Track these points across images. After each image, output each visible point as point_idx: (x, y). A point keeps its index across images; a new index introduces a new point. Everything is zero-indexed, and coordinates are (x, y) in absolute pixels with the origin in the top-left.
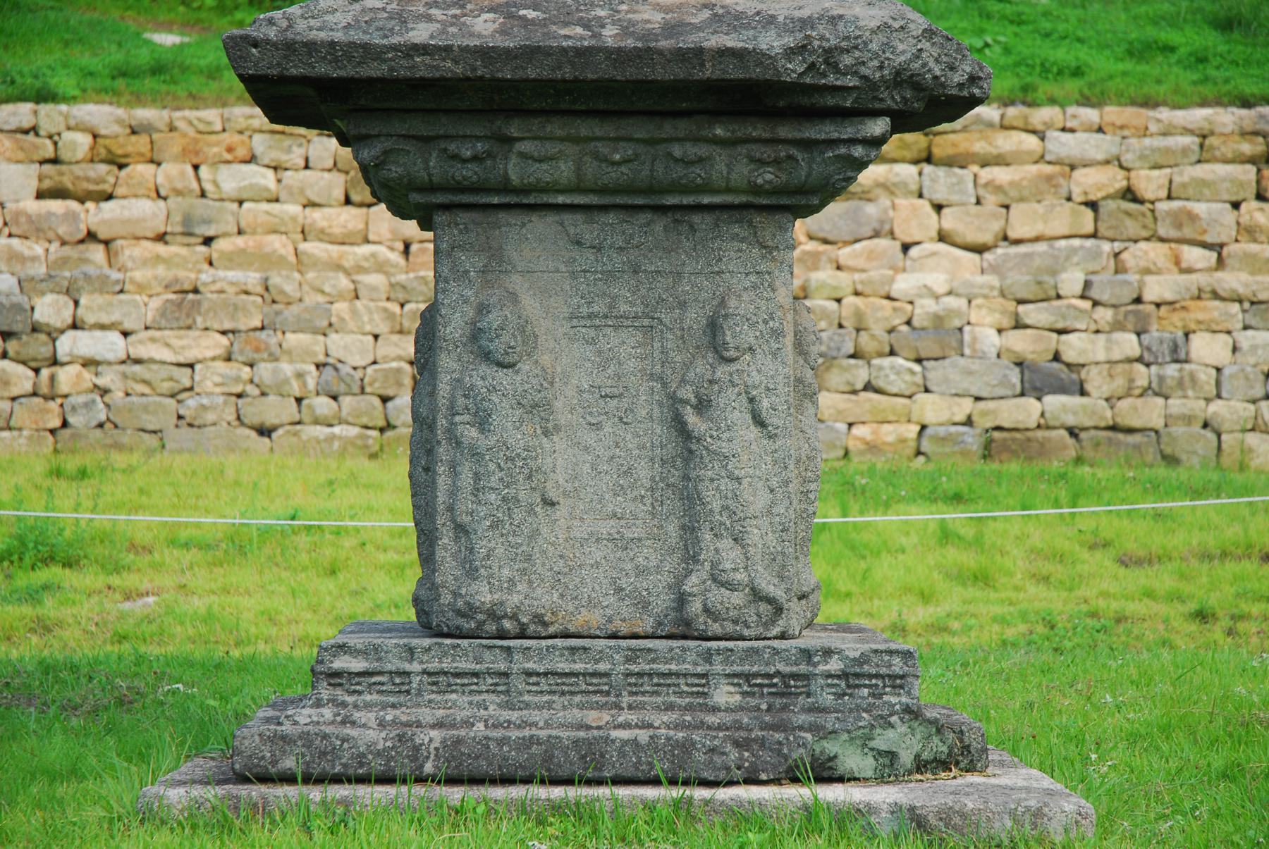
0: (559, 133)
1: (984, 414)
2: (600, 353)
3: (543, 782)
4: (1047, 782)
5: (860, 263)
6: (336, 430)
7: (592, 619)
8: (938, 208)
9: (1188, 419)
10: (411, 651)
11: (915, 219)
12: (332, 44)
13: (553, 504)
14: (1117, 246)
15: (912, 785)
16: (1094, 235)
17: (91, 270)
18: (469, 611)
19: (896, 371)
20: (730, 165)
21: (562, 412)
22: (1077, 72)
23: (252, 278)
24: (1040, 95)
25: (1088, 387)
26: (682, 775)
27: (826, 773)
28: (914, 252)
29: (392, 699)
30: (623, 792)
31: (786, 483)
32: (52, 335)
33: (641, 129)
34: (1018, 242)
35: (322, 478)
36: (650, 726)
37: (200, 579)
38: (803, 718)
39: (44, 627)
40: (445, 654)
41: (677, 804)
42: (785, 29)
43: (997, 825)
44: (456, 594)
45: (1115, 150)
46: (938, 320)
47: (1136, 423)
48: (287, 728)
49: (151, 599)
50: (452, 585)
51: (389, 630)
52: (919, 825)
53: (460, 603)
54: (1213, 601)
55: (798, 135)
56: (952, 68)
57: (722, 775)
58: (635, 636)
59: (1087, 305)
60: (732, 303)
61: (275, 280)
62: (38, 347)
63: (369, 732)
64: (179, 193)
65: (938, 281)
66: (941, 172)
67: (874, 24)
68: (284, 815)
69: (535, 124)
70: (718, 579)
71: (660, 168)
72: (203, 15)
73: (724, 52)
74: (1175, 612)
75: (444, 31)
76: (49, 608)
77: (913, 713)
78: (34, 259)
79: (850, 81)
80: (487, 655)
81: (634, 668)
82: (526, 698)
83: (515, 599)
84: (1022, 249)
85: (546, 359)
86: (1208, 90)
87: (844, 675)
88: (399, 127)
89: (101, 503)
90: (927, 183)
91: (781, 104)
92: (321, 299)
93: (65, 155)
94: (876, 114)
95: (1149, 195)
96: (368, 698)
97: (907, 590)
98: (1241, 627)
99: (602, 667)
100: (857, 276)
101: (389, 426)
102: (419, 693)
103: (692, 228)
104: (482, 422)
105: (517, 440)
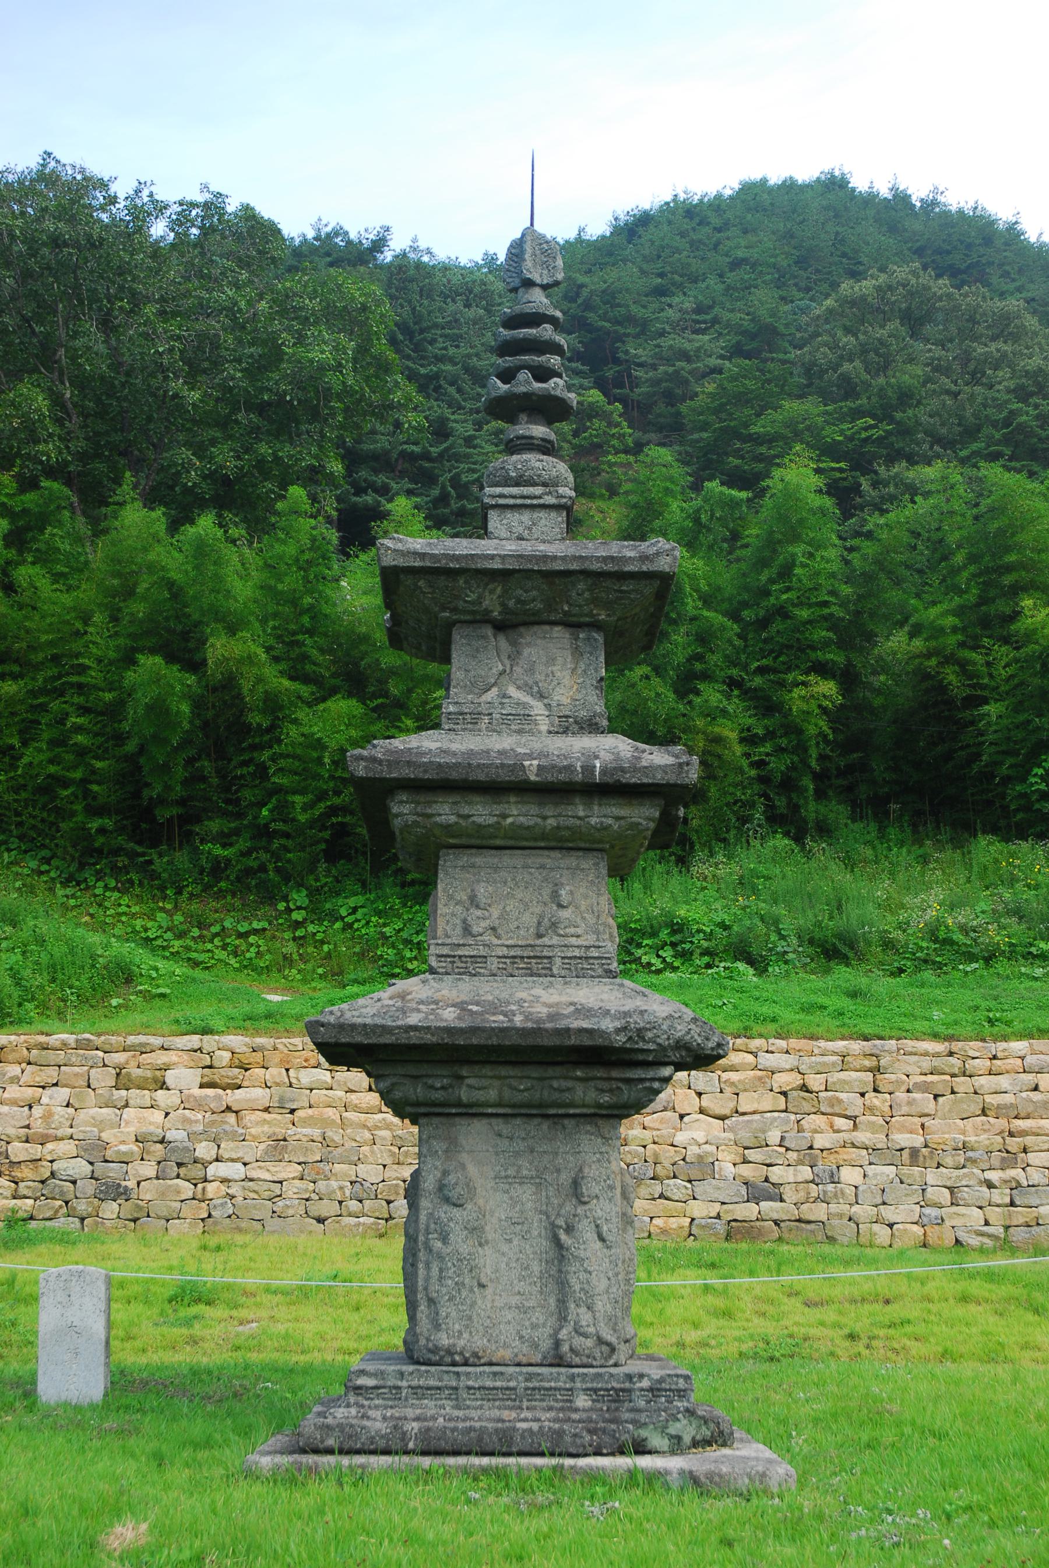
0: (490, 1074)
2: (511, 1198)
3: (477, 1454)
4: (768, 1454)
5: (656, 1125)
6: (361, 1220)
7: (506, 1354)
8: (699, 1094)
9: (840, 1216)
10: (402, 1374)
12: (365, 1025)
13: (484, 1286)
14: (799, 1117)
16: (786, 1111)
17: (227, 1128)
18: (435, 1350)
19: (677, 1187)
22: (774, 1020)
23: (316, 1133)
25: (784, 1197)
26: (557, 1450)
27: (641, 1449)
28: (686, 1119)
29: (390, 1403)
30: (524, 1461)
31: (617, 1274)
32: (205, 1164)
33: (535, 1072)
34: (744, 1114)
35: (353, 1251)
36: (539, 1420)
37: (282, 1313)
38: (627, 1416)
39: (193, 1341)
41: (555, 1469)
42: (615, 1018)
44: (428, 1340)
45: (796, 1063)
46: (700, 1157)
47: (812, 1218)
48: (330, 1420)
49: (254, 1325)
50: (426, 1333)
51: (389, 1359)
52: (695, 1482)
53: (430, 1345)
54: (858, 1328)
55: (623, 1076)
56: (708, 1039)
57: (581, 1450)
58: (531, 1365)
59: (783, 1150)
60: (586, 1170)
61: (329, 1134)
62: (197, 1171)
63: (377, 1425)
64: (278, 1084)
65: (700, 1136)
67: (664, 1015)
69: (476, 1068)
70: (578, 1331)
71: (546, 1093)
72: (294, 984)
74: (837, 1334)
75: (426, 1018)
76: (197, 1330)
77: (690, 1412)
78: (197, 1121)
79: (652, 1046)
80: (446, 1377)
83: (462, 1343)
84: (746, 1118)
85: (481, 1202)
87: (651, 1390)
88: (401, 1070)
89: (228, 1267)
90: (692, 1080)
91: (613, 1058)
92: (354, 1144)
93: (216, 1064)
94: (666, 1064)
95: (815, 1089)
96: (377, 1402)
97: (685, 1321)
98: (874, 1343)
99: (512, 1384)
100: (655, 1133)
101: (391, 1218)
102: (406, 1399)
103: (564, 1127)
104: (445, 1239)
105: (464, 1249)
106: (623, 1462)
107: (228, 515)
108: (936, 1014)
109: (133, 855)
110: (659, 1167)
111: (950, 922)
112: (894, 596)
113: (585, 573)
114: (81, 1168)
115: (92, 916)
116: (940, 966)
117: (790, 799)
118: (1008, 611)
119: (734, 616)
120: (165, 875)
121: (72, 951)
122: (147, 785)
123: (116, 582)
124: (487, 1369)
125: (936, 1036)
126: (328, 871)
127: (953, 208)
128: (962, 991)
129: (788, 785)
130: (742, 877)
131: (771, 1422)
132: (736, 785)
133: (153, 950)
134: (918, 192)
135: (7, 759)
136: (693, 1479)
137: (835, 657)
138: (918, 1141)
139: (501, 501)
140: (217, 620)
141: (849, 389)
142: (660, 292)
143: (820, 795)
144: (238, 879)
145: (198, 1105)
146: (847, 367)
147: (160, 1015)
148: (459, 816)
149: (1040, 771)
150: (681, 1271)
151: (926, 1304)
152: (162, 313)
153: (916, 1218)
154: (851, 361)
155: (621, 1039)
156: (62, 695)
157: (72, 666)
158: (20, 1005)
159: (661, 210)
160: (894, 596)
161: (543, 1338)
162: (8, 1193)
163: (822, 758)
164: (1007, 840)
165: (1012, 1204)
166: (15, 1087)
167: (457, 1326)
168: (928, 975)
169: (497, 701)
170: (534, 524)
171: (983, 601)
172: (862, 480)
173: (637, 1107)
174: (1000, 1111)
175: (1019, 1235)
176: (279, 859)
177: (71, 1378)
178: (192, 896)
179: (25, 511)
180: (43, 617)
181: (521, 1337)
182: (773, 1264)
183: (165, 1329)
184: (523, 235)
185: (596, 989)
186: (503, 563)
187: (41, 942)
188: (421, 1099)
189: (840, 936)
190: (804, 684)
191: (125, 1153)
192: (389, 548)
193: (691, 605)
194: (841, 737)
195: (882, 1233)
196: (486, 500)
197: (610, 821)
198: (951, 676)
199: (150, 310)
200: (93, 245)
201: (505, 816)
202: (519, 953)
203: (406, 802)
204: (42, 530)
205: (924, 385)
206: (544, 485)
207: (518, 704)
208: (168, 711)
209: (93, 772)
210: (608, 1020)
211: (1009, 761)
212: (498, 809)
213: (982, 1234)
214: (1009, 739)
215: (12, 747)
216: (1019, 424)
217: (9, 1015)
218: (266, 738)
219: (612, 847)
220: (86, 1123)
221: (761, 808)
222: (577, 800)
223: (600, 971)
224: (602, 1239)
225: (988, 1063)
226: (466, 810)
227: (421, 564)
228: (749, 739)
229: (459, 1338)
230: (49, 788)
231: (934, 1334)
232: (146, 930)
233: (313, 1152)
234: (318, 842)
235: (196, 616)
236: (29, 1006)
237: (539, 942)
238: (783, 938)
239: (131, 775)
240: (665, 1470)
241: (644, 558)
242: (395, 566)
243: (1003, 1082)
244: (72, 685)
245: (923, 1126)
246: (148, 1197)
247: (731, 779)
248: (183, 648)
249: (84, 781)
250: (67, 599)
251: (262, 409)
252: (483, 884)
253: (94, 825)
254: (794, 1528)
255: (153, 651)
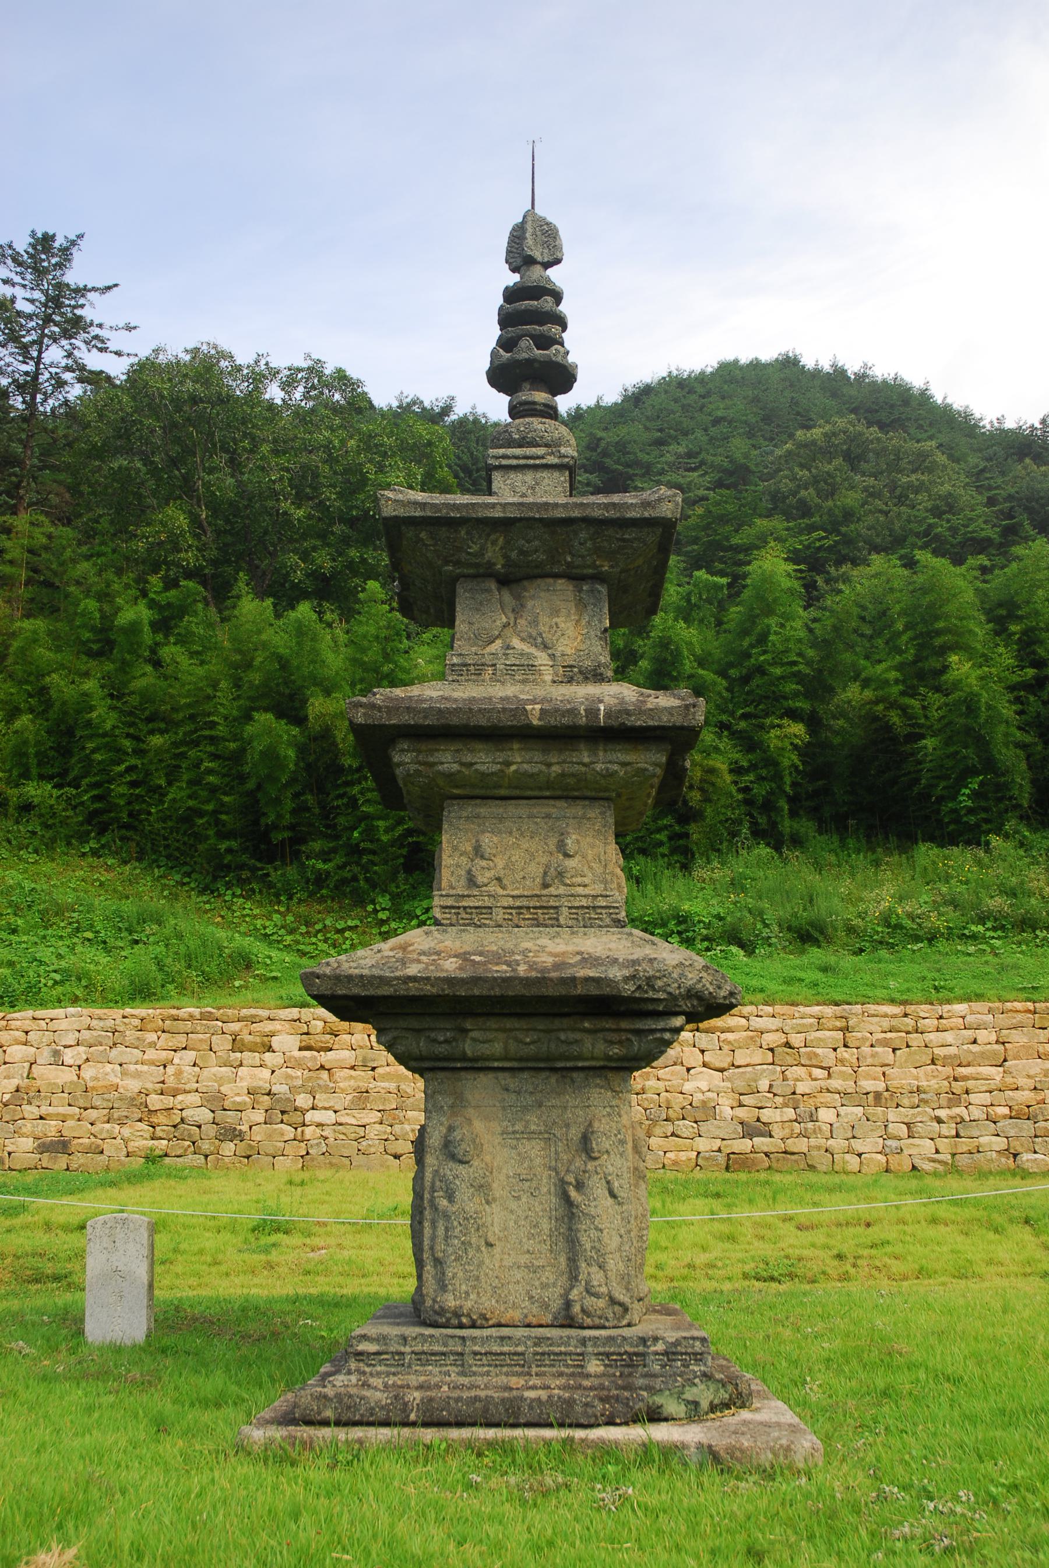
0: (494, 1026)
1: (726, 1146)
2: (519, 1154)
5: (668, 1077)
7: (516, 1315)
8: (703, 1052)
9: (819, 1148)
10: (404, 1339)
11: (692, 1057)
12: (362, 976)
15: (709, 1424)
17: (321, 1082)
18: (442, 1312)
19: (685, 1127)
20: (593, 1043)
21: (497, 1191)
22: (762, 991)
24: (746, 1000)
27: (655, 1416)
29: (393, 1370)
30: (531, 1433)
31: (629, 1232)
33: (541, 1024)
34: (739, 1067)
36: (549, 1387)
38: (641, 1382)
39: (270, 1266)
40: (426, 1341)
43: (763, 1457)
44: (434, 1301)
48: (329, 1391)
54: (845, 1249)
55: (632, 1027)
56: (720, 988)
57: (592, 1420)
58: (541, 1326)
60: (596, 1124)
61: (403, 1087)
62: (297, 1118)
64: (361, 1047)
65: (704, 1086)
66: (703, 1035)
68: (321, 1450)
70: (589, 1291)
71: (553, 1046)
73: (588, 980)
74: (825, 1255)
75: (426, 969)
76: (274, 1256)
77: (707, 1376)
79: (662, 995)
80: (451, 1342)
81: (539, 1350)
82: (474, 1369)
83: (469, 1304)
86: (819, 998)
87: (666, 1353)
91: (622, 1009)
93: (311, 1031)
94: (677, 1014)
96: (379, 1368)
97: (695, 1245)
98: (859, 1262)
99: (520, 1349)
102: (410, 1366)
103: (573, 1081)
104: (450, 1197)
105: (471, 1207)
106: (636, 1433)
107: (326, 605)
108: (892, 984)
109: (254, 870)
110: (670, 1111)
111: (900, 911)
112: (847, 657)
113: (586, 521)
114: (204, 1115)
115: (223, 917)
116: (892, 946)
117: (770, 817)
118: (938, 666)
119: (723, 674)
120: (279, 885)
121: (204, 944)
122: (264, 814)
123: (238, 657)
124: (493, 1332)
125: (893, 1001)
126: (406, 880)
127: (880, 379)
128: (910, 966)
129: (768, 806)
130: (733, 879)
131: (784, 1364)
132: (726, 807)
133: (270, 943)
134: (852, 367)
135: (157, 796)
136: (712, 1455)
137: (801, 704)
138: (880, 1086)
139: (504, 462)
140: (315, 685)
141: (805, 510)
142: (660, 443)
143: (793, 814)
144: (336, 887)
145: (298, 1064)
146: (803, 493)
147: (269, 994)
148: (462, 764)
149: (967, 791)
150: (691, 1200)
151: (901, 1227)
152: (276, 452)
153: (880, 1149)
154: (807, 489)
155: (629, 989)
156: (197, 745)
157: (205, 723)
158: (163, 986)
159: (659, 383)
160: (847, 657)
161: (554, 1297)
162: (147, 1135)
163: (794, 784)
164: (942, 846)
165: (958, 1136)
166: (153, 1050)
167: (464, 1287)
168: (883, 953)
169: (500, 652)
170: (537, 484)
171: (918, 659)
172: (818, 578)
173: (647, 1059)
174: (946, 1061)
175: (963, 1160)
176: (367, 871)
177: (116, 1320)
178: (300, 901)
179: (169, 605)
180: (183, 685)
181: (531, 1297)
182: (769, 1194)
183: (246, 1256)
184: (525, 217)
185: (604, 939)
186: (504, 512)
187: (180, 936)
188: (424, 1053)
189: (812, 924)
190: (779, 726)
191: (239, 1103)
192: (389, 499)
193: (688, 665)
194: (809, 768)
195: (853, 1162)
196: (490, 461)
197: (616, 767)
198: (895, 718)
199: (265, 448)
200: (222, 401)
201: (508, 764)
202: (525, 904)
203: (408, 751)
204: (181, 618)
205: (863, 506)
206: (546, 446)
207: (522, 654)
208: (278, 757)
209: (223, 804)
210: (616, 968)
211: (943, 784)
212: (500, 756)
213: (934, 1161)
214: (942, 766)
215: (160, 787)
216: (936, 535)
217: (154, 994)
218: (356, 776)
219: (619, 795)
220: (210, 1079)
221: (747, 825)
222: (582, 746)
223: (608, 921)
224: (613, 1195)
225: (936, 1022)
226: (468, 758)
227: (422, 514)
228: (737, 770)
229: (466, 1299)
230: (188, 817)
231: (910, 1253)
232: (265, 928)
233: (390, 1102)
234: (398, 857)
235: (299, 683)
236: (170, 987)
237: (545, 892)
238: (766, 926)
239: (251, 807)
240: (682, 1443)
241: (645, 504)
242: (396, 517)
243: (948, 1037)
244: (206, 737)
245: (884, 1074)
246: (258, 1138)
247: (722, 802)
248: (290, 707)
249: (215, 812)
250: (200, 671)
251: (352, 522)
252: (488, 835)
253: (223, 846)
254: (827, 1524)
255: (266, 710)
